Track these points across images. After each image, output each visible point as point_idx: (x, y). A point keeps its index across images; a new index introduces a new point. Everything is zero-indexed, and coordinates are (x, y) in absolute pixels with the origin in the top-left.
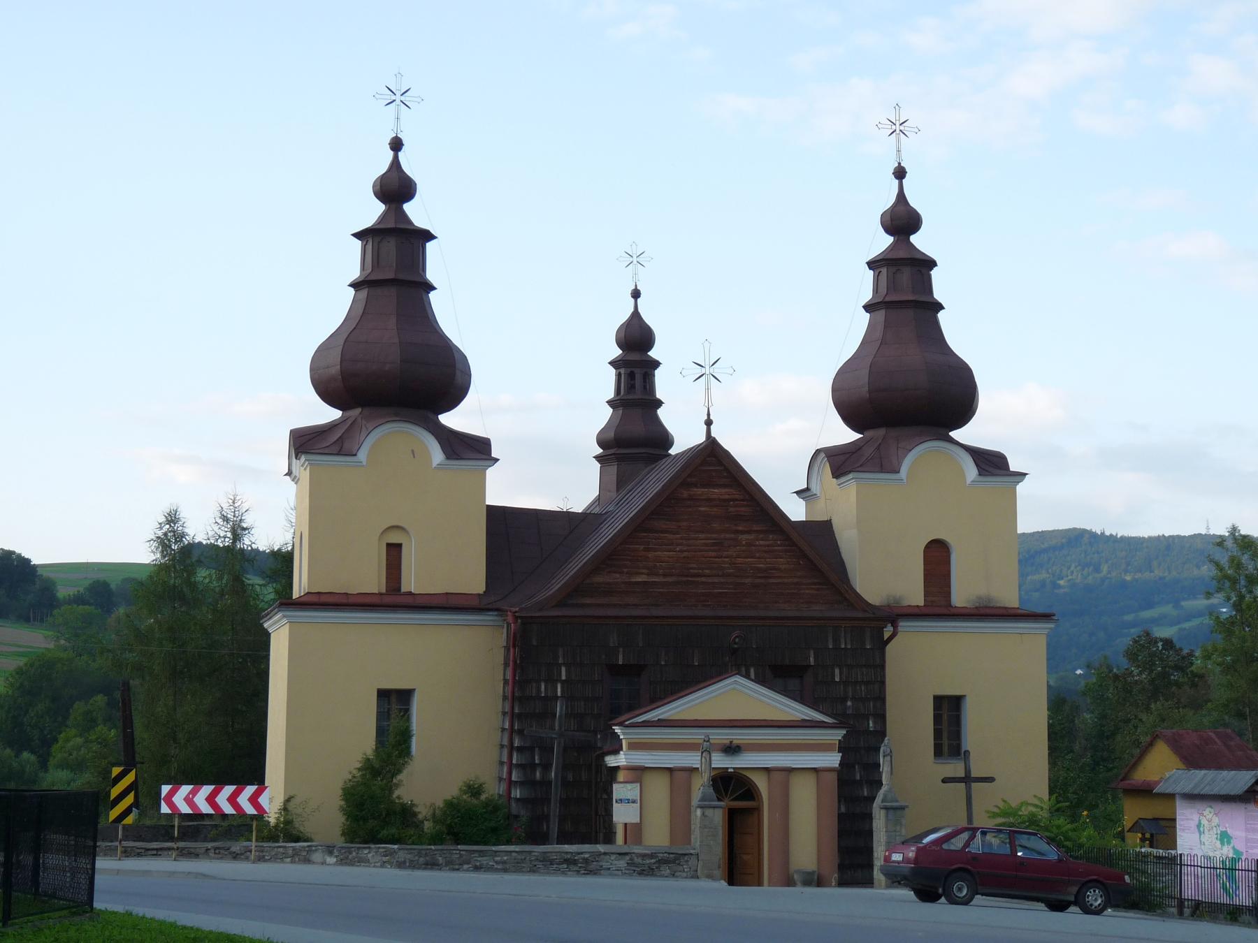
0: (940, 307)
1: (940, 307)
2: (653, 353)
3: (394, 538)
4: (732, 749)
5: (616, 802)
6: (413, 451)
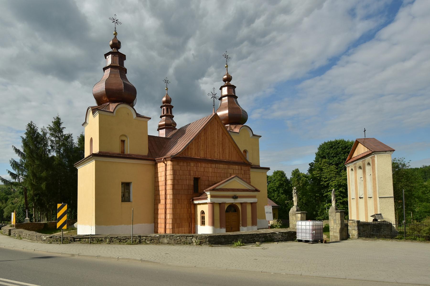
0: (237, 97)
1: (237, 97)
2: (172, 104)
3: (123, 138)
4: (235, 197)
5: (266, 213)
6: (128, 114)
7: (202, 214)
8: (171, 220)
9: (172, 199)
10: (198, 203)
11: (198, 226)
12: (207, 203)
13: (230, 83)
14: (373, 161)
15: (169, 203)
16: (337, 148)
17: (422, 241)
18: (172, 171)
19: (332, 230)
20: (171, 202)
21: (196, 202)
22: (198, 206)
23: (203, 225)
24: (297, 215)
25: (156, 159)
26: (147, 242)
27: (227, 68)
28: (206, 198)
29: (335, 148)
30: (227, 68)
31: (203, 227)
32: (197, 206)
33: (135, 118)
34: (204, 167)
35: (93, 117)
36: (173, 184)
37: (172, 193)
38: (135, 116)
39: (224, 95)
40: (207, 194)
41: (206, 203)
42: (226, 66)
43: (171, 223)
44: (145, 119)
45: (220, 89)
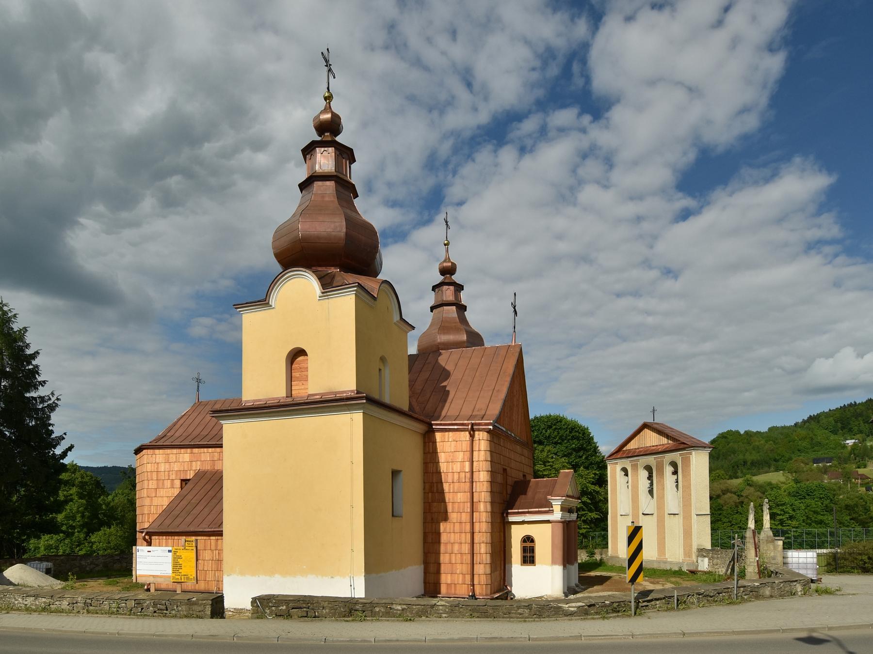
7: (523, 542)
8: (488, 556)
9: (490, 513)
10: (521, 520)
11: (512, 567)
12: (549, 520)
13: (453, 277)
14: (687, 461)
15: (484, 520)
16: (559, 429)
17: (858, 573)
18: (488, 453)
19: (752, 564)
20: (488, 519)
21: (512, 519)
22: (513, 526)
23: (529, 564)
24: (777, 543)
25: (432, 422)
26: (744, 596)
27: (448, 248)
28: (551, 512)
29: (556, 429)
30: (448, 248)
31: (529, 568)
32: (511, 529)
33: (397, 321)
34: (431, 443)
35: (320, 297)
36: (491, 482)
37: (490, 499)
38: (397, 318)
39: (447, 301)
40: (553, 504)
41: (548, 522)
42: (446, 242)
43: (489, 561)
44: (407, 326)
45: (434, 288)
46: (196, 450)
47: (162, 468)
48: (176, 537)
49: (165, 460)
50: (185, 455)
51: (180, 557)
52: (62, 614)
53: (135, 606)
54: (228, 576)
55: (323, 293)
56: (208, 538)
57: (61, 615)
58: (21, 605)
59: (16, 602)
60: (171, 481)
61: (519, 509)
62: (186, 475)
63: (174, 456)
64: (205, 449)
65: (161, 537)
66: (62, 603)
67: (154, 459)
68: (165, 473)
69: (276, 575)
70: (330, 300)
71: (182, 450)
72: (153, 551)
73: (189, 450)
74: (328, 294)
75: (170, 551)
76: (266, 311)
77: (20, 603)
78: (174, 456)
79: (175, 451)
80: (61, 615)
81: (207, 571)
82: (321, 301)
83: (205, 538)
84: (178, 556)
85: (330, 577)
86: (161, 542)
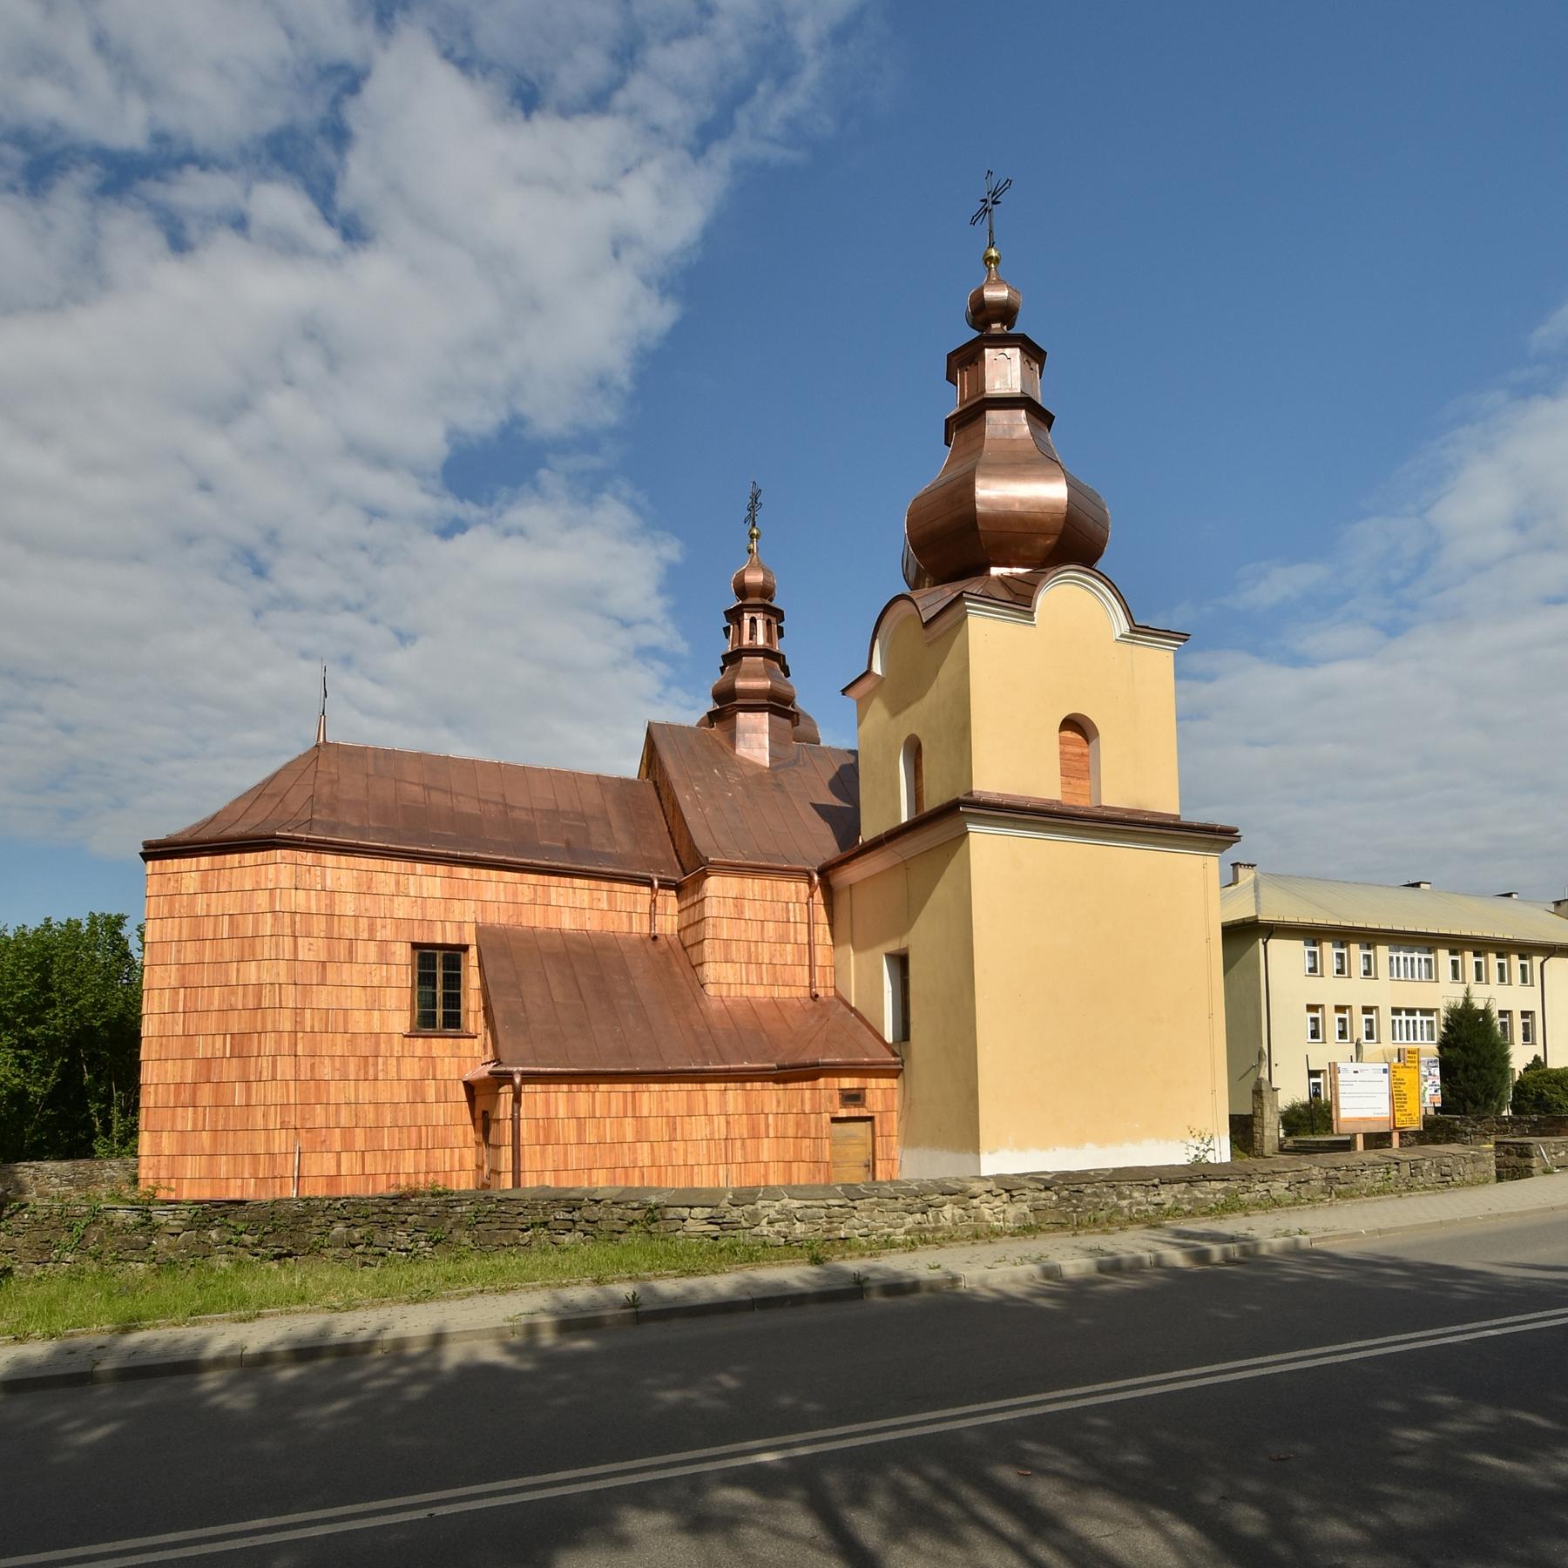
35: (1122, 636)
46: (465, 872)
47: (347, 905)
48: (602, 1087)
49: (359, 885)
50: (429, 881)
51: (1401, 1082)
52: (1412, 1194)
53: (1411, 1173)
54: (990, 1153)
55: (1131, 631)
56: (698, 1086)
57: (1410, 1196)
58: (1142, 1208)
59: (1124, 1203)
60: (380, 947)
61: (729, 1064)
62: (431, 930)
63: (391, 879)
64: (484, 872)
65: (552, 1087)
66: (1270, 1186)
67: (319, 880)
68: (356, 923)
69: (1088, 1145)
70: (1134, 647)
71: (419, 867)
72: (1362, 1070)
73: (441, 869)
74: (1139, 636)
75: (1385, 1071)
76: (1005, 623)
77: (1139, 1204)
78: (391, 879)
79: (394, 865)
80: (1410, 1196)
81: (696, 1167)
82: (1120, 644)
83: (689, 1086)
84: (1399, 1079)
85: (1178, 1141)
86: (552, 1100)
